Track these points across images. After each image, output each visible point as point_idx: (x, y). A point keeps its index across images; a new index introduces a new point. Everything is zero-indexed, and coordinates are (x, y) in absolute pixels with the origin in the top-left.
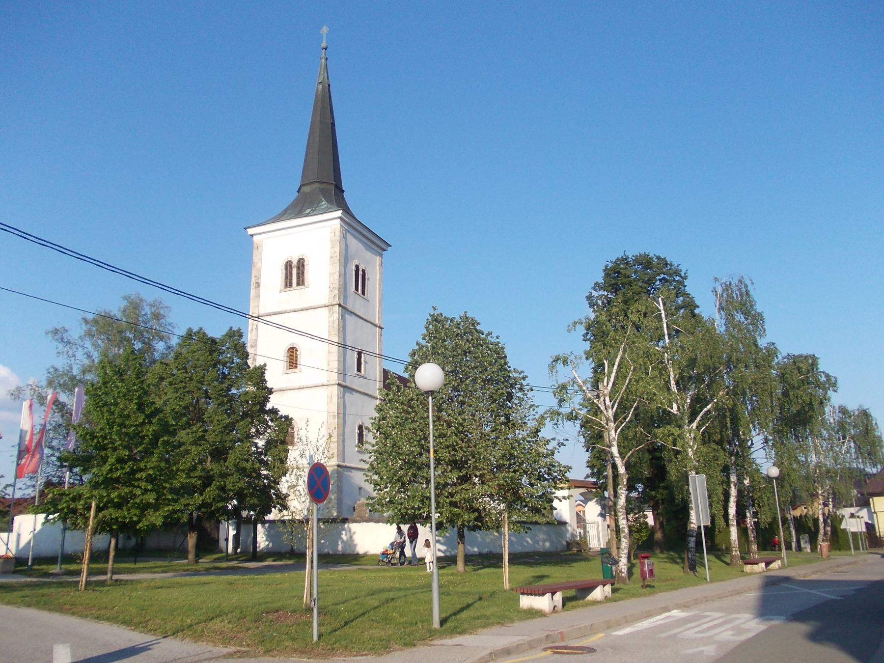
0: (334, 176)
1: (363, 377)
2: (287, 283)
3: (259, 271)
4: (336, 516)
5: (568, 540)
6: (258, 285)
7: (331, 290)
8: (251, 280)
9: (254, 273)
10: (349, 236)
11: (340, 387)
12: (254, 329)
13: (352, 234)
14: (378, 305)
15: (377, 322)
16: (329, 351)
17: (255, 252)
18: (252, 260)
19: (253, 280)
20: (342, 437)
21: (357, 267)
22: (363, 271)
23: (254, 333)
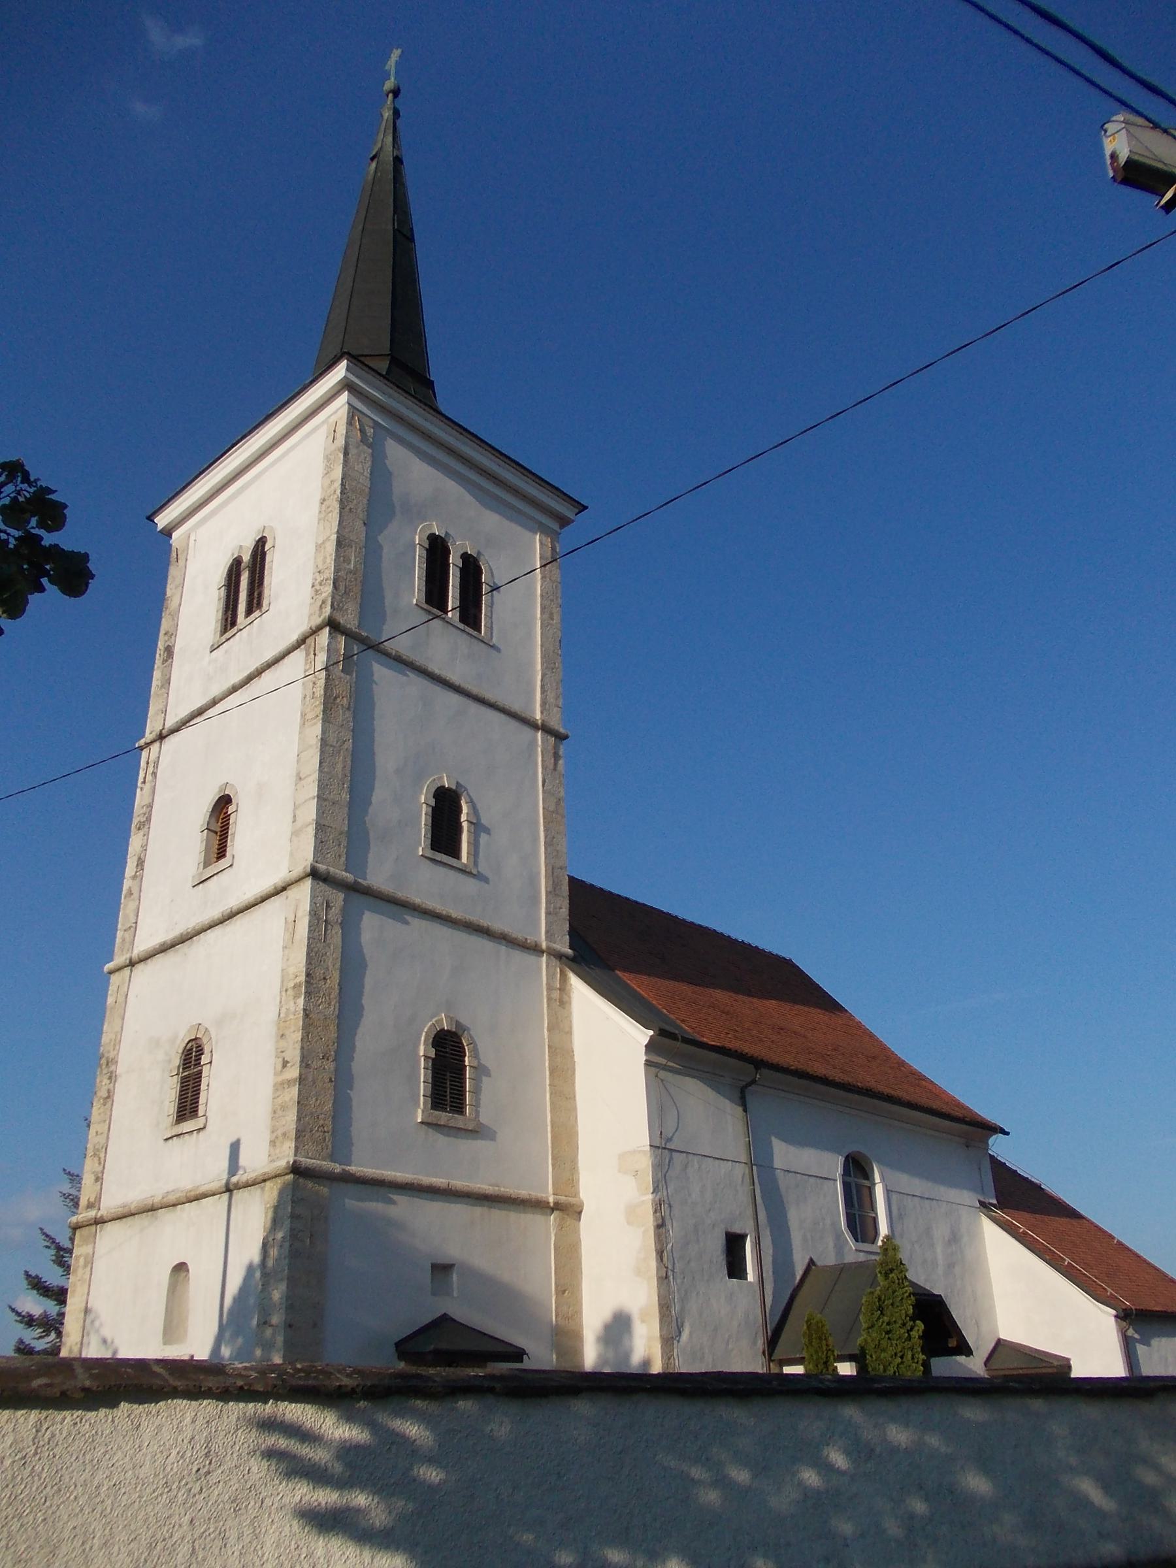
0: (392, 341)
1: (463, 871)
2: (226, 620)
3: (175, 616)
4: (257, 1348)
5: (133, 956)
6: (169, 651)
7: (317, 591)
8: (157, 645)
9: (165, 625)
10: (395, 452)
11: (322, 886)
12: (149, 778)
13: (401, 441)
14: (539, 667)
15: (538, 716)
16: (298, 774)
17: (173, 571)
18: (165, 594)
19: (161, 645)
20: (330, 1066)
21: (437, 549)
22: (471, 567)
23: (147, 786)
